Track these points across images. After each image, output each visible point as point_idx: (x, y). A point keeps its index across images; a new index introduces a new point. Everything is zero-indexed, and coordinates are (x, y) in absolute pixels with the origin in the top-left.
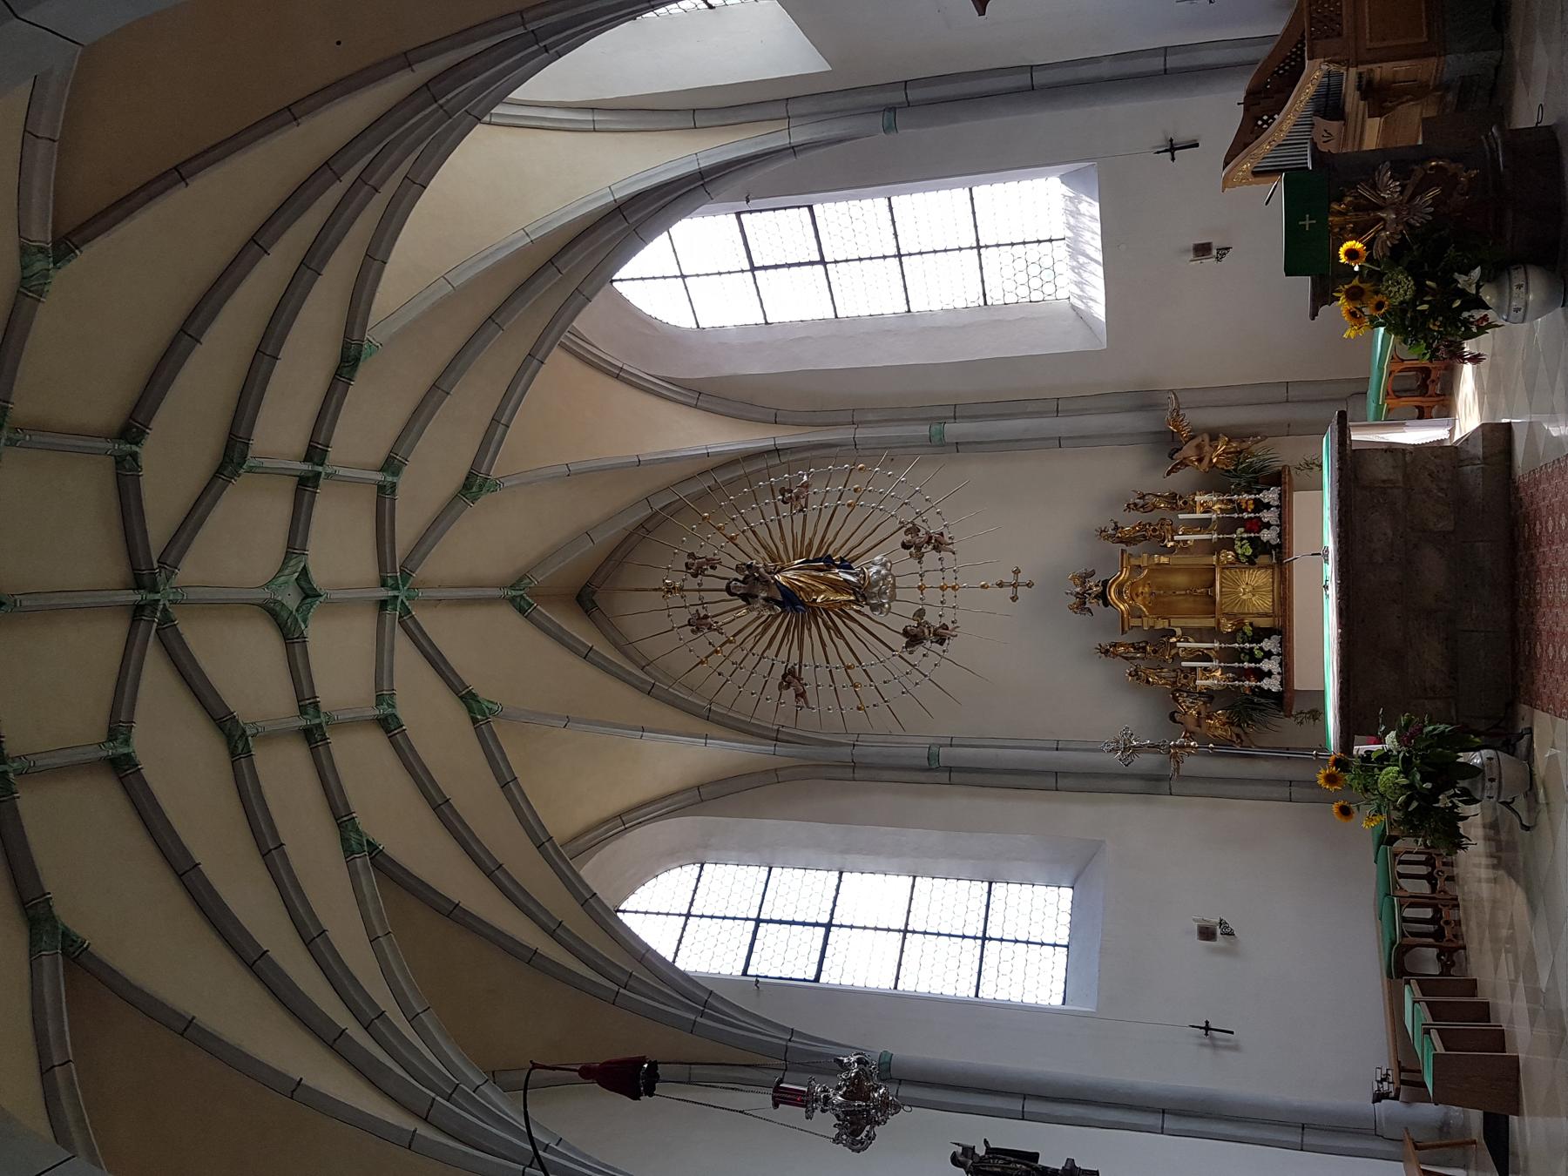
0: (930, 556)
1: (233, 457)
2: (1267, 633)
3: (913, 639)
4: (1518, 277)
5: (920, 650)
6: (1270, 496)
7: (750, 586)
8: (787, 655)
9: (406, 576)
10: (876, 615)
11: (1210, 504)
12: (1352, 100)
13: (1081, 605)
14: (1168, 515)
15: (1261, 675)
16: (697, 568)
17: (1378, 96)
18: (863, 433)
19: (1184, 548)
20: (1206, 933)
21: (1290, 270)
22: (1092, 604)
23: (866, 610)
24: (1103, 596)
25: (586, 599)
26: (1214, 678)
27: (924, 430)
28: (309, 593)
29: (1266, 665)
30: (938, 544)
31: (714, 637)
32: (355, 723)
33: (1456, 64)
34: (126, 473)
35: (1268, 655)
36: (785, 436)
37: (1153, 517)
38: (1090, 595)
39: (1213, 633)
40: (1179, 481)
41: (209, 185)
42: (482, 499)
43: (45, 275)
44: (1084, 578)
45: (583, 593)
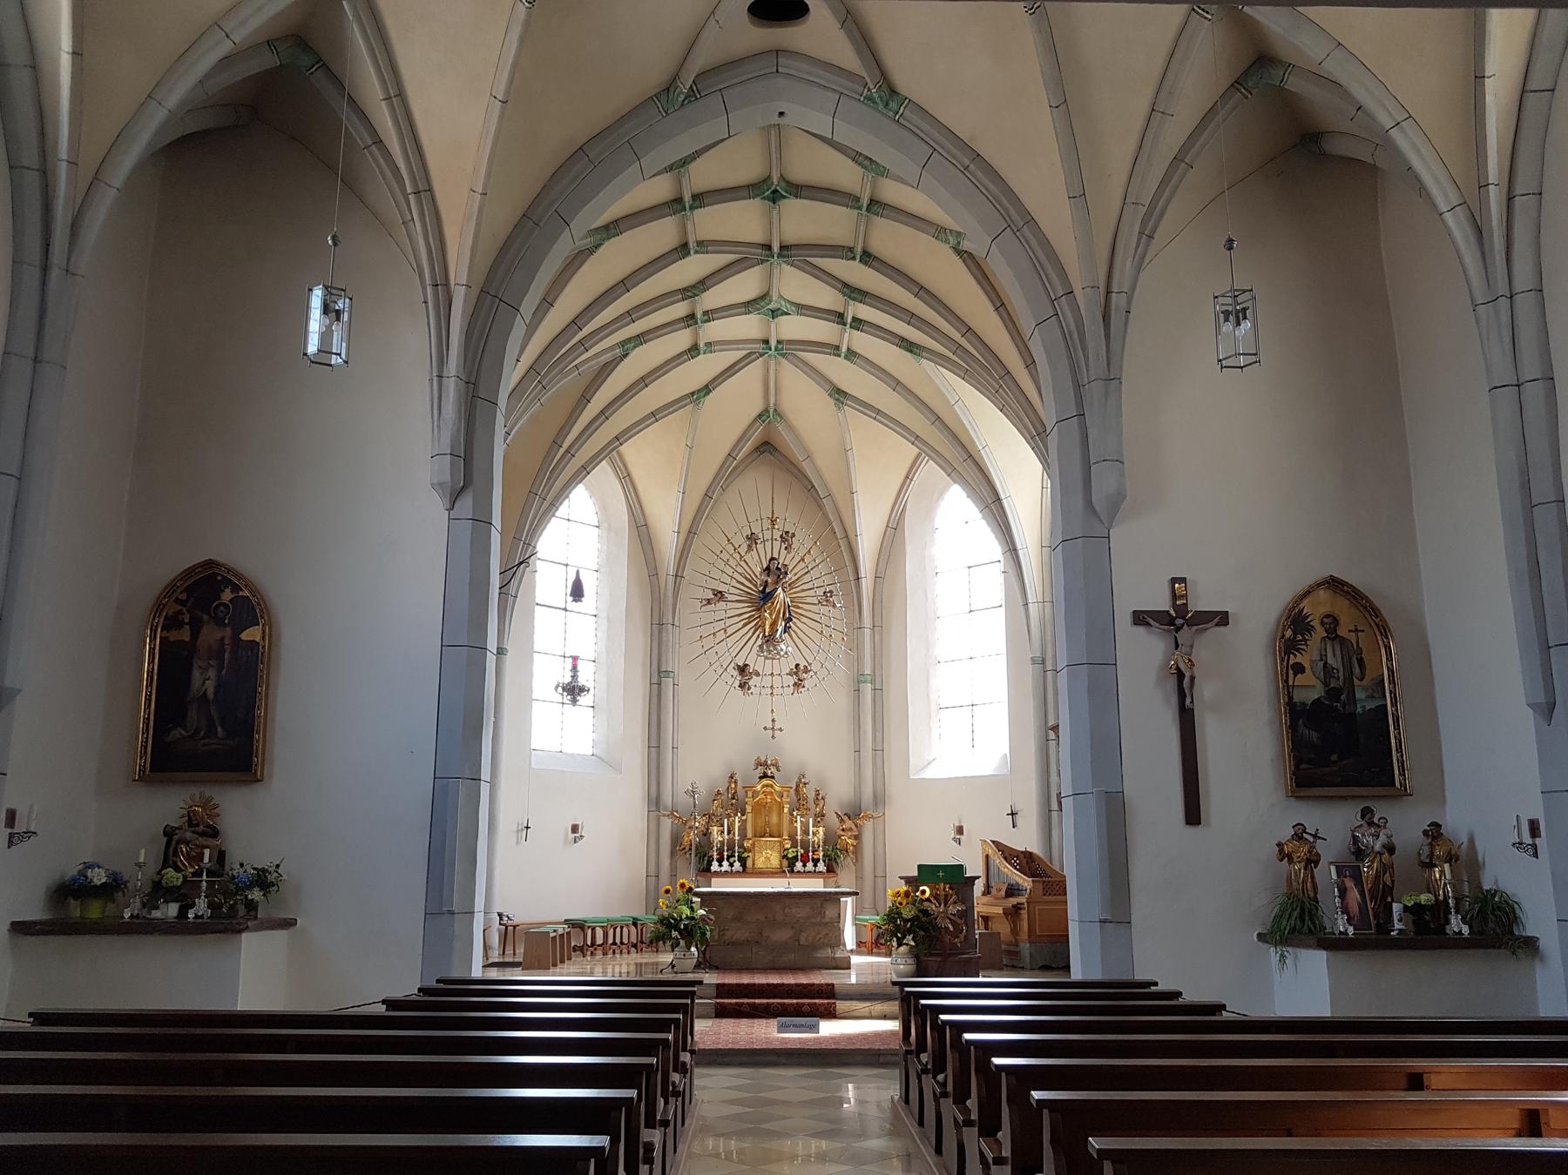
0: (792, 680)
1: (854, 293)
2: (744, 865)
3: (742, 670)
4: (910, 961)
5: (736, 673)
6: (821, 867)
7: (775, 571)
8: (732, 593)
9: (783, 355)
10: (756, 648)
11: (818, 835)
12: (1014, 901)
13: (759, 764)
14: (812, 813)
15: (720, 861)
16: (786, 538)
17: (1013, 913)
18: (867, 632)
19: (792, 821)
20: (575, 829)
21: (920, 867)
22: (760, 770)
23: (759, 642)
24: (765, 776)
25: (767, 447)
26: (717, 836)
27: (867, 671)
28: (775, 313)
29: (725, 863)
30: (798, 685)
31: (744, 548)
32: (696, 335)
33: (1025, 948)
34: (846, 252)
35: (731, 865)
36: (867, 584)
37: (811, 804)
38: (766, 771)
39: (743, 836)
40: (832, 819)
41: (995, 320)
42: (832, 402)
43: (947, 241)
44: (776, 765)
45: (768, 447)
